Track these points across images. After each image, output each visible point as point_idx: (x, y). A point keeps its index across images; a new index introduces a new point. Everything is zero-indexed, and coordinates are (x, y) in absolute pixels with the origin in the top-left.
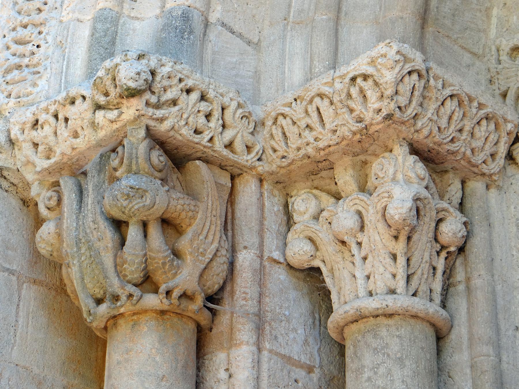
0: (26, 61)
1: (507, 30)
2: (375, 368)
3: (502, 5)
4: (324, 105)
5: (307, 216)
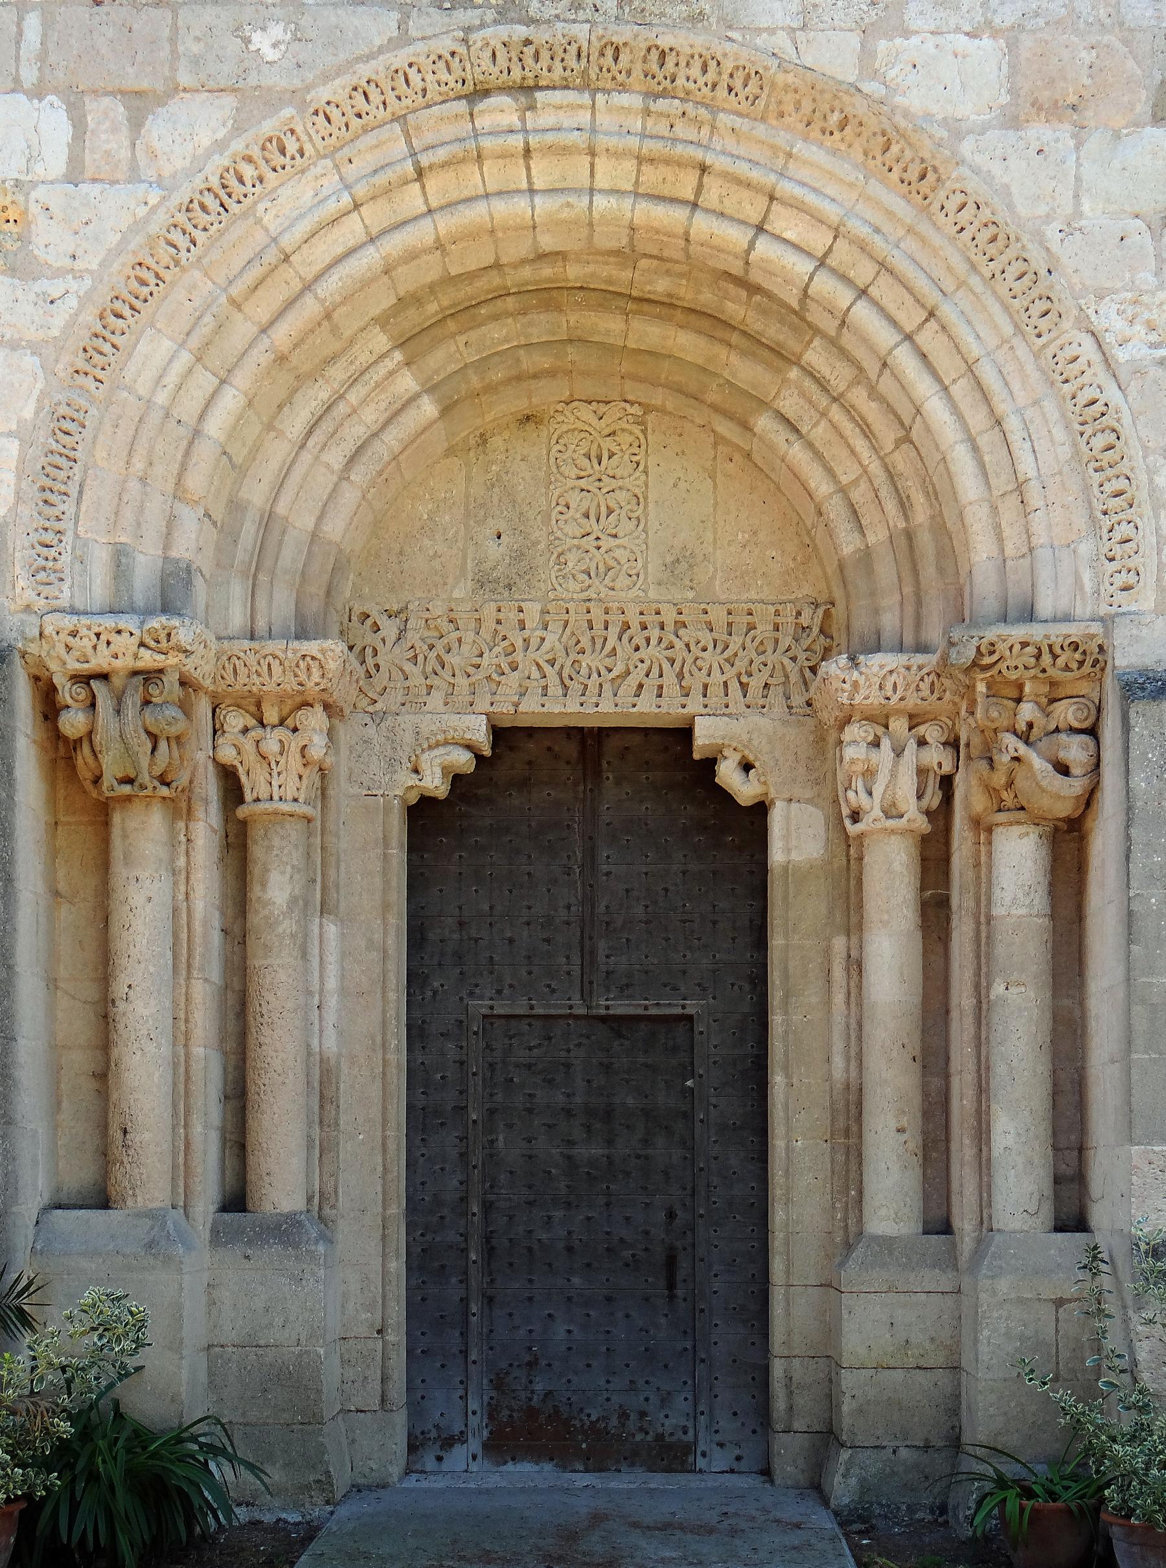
0: (50, 564)
2: (282, 849)
4: (275, 665)
5: (236, 730)
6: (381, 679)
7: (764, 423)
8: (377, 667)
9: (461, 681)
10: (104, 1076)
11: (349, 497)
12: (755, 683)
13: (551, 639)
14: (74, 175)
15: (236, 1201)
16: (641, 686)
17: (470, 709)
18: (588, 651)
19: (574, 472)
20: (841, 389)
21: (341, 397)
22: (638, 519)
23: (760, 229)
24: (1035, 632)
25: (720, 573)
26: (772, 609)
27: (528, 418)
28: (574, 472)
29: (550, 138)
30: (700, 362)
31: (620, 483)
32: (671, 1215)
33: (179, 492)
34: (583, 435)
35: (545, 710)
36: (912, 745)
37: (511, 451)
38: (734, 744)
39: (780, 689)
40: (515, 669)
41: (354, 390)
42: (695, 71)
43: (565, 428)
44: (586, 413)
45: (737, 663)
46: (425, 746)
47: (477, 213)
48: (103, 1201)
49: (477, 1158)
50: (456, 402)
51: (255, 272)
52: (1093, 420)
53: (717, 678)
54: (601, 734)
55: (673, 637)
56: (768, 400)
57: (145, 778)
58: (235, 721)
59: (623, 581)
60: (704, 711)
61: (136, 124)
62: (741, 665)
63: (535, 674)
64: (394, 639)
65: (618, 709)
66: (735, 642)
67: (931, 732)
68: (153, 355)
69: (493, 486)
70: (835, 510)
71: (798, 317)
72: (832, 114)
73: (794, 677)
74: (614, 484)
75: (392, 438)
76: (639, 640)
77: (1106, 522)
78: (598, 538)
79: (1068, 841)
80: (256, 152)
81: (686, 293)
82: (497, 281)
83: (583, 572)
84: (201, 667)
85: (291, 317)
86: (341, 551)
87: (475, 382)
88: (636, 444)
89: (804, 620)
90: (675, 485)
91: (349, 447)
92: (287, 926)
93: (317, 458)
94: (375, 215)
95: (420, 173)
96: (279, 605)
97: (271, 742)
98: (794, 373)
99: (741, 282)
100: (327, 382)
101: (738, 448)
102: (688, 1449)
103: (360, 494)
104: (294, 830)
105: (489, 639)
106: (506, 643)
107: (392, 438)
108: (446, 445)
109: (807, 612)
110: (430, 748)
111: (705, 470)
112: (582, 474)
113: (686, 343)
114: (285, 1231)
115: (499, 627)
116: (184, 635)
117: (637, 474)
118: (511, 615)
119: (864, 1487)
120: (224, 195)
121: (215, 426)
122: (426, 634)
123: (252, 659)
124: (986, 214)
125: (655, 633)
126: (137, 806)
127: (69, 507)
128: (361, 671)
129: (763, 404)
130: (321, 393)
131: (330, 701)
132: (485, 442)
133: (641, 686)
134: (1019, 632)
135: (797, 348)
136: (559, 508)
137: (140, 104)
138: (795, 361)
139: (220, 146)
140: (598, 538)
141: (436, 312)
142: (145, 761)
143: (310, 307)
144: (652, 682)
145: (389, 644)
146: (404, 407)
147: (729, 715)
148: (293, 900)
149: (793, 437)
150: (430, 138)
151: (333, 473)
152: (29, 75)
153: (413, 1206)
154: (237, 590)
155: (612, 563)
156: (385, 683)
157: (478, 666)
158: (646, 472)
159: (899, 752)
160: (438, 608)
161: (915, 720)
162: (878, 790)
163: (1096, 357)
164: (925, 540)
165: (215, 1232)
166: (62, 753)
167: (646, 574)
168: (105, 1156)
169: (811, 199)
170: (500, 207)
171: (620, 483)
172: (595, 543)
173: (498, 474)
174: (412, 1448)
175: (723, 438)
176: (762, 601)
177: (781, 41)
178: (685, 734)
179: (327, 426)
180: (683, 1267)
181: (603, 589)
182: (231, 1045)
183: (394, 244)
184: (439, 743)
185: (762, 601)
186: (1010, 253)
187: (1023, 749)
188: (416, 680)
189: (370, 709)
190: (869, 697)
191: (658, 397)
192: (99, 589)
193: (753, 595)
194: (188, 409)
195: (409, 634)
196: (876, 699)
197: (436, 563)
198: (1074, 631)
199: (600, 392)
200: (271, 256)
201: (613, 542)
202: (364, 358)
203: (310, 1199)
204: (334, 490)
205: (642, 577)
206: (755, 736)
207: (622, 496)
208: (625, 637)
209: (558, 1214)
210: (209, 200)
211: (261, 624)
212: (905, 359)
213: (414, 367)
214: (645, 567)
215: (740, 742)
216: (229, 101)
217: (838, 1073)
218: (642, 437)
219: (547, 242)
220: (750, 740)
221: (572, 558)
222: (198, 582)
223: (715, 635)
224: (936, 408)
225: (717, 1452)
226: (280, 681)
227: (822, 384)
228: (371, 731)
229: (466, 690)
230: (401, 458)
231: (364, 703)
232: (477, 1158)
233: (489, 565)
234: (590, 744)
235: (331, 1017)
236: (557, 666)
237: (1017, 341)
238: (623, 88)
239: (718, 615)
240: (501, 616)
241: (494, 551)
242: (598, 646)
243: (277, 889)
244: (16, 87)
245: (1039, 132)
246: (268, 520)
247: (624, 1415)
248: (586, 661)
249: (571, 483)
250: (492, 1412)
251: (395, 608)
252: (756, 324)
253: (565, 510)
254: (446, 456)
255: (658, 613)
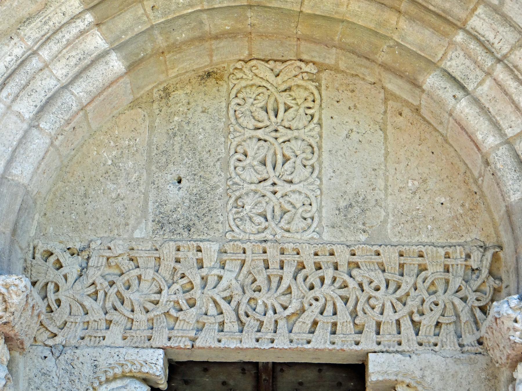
1: (44, 235)
3: (42, 214)
6: (61, 315)
7: (432, 81)
8: (59, 302)
9: (140, 316)
11: (38, 143)
12: (427, 322)
13: (228, 277)
16: (315, 323)
17: (147, 344)
18: (264, 289)
19: (252, 123)
20: (505, 51)
21: (35, 53)
22: (313, 167)
25: (391, 218)
26: (442, 252)
27: (209, 74)
28: (252, 123)
30: (372, 26)
31: (296, 133)
34: (261, 90)
35: (221, 345)
37: (193, 104)
38: (407, 381)
39: (452, 328)
40: (192, 306)
41: (47, 47)
43: (243, 83)
45: (409, 302)
46: (103, 379)
50: (142, 60)
53: (390, 316)
54: (276, 369)
55: (346, 277)
56: (436, 62)
59: (298, 224)
60: (378, 348)
62: (413, 304)
63: (212, 310)
64: (75, 276)
65: (294, 346)
66: (407, 282)
69: (175, 135)
73: (465, 317)
74: (290, 134)
75: (81, 90)
76: (314, 279)
78: (274, 184)
83: (260, 215)
86: (27, 193)
87: (161, 41)
88: (310, 99)
89: (474, 263)
90: (348, 136)
91: (40, 98)
93: (9, 107)
98: (460, 37)
100: (22, 39)
101: (407, 103)
103: (48, 141)
105: (168, 276)
106: (184, 281)
107: (81, 90)
108: (131, 98)
109: (476, 255)
110: (108, 381)
111: (376, 122)
112: (260, 125)
115: (178, 266)
117: (312, 126)
118: (190, 254)
122: (107, 271)
125: (329, 273)
128: (42, 306)
129: (431, 64)
131: (12, 334)
132: (168, 95)
133: (315, 323)
135: (463, 15)
136: (238, 156)
140: (274, 184)
144: (327, 318)
145: (71, 280)
146: (93, 62)
147: (401, 353)
149: (459, 94)
151: (23, 121)
155: (288, 207)
156: (65, 317)
157: (157, 303)
158: (320, 124)
160: (120, 247)
167: (320, 217)
171: (296, 133)
172: (272, 188)
173: (180, 124)
175: (393, 94)
176: (433, 245)
178: (357, 371)
179: (20, 79)
181: (278, 231)
185: (433, 245)
188: (96, 314)
189: (50, 342)
191: (331, 57)
193: (424, 239)
195: (91, 271)
197: (119, 206)
199: (278, 52)
201: (288, 188)
204: (24, 137)
205: (316, 220)
206: (427, 373)
207: (296, 145)
208: (300, 277)
213: (103, 27)
214: (319, 211)
215: (413, 378)
218: (316, 92)
220: (423, 377)
221: (249, 202)
223: (387, 275)
227: (487, 47)
228: (51, 363)
229: (144, 325)
230: (88, 108)
233: (170, 207)
236: (234, 304)
239: (389, 256)
240: (180, 255)
241: (174, 194)
242: (274, 285)
248: (261, 298)
249: (248, 133)
251: (78, 246)
253: (242, 157)
254: (131, 108)
255: (332, 254)
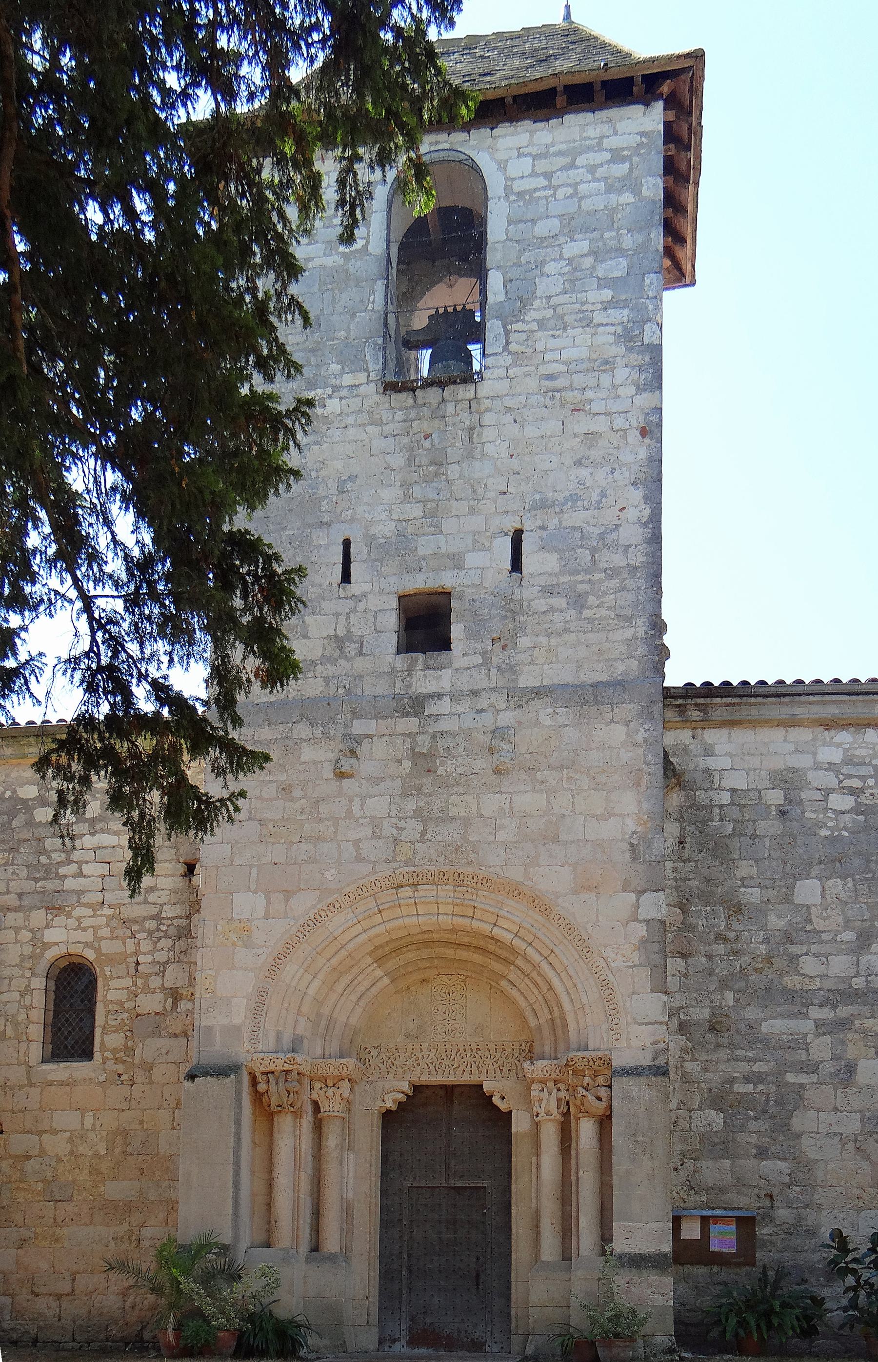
6: (371, 1070)
10: (269, 1205)
11: (359, 1010)
12: (505, 1069)
13: (432, 1055)
14: (266, 917)
15: (315, 1248)
23: (495, 925)
24: (587, 1054)
29: (423, 900)
32: (478, 1259)
33: (299, 1012)
36: (555, 1090)
42: (470, 878)
44: (444, 978)
47: (400, 922)
48: (268, 1245)
49: (406, 1238)
51: (325, 943)
52: (604, 985)
57: (285, 1105)
58: (318, 1085)
61: (287, 901)
66: (498, 1056)
67: (562, 1086)
68: (291, 970)
70: (528, 1012)
71: (512, 949)
72: (515, 891)
75: (373, 991)
77: (610, 1018)
79: (605, 1122)
80: (326, 908)
81: (475, 942)
82: (409, 939)
84: (306, 1068)
85: (337, 956)
87: (403, 971)
92: (335, 1154)
94: (366, 924)
95: (380, 912)
96: (334, 1046)
97: (330, 1093)
98: (512, 967)
99: (493, 938)
102: (484, 1344)
104: (338, 1122)
107: (373, 991)
113: (477, 958)
114: (331, 1258)
116: (299, 1059)
119: (537, 1348)
120: (315, 920)
121: (311, 992)
123: (323, 1065)
124: (567, 921)
125: (469, 1053)
126: (283, 1114)
127: (262, 1019)
130: (349, 977)
134: (581, 1054)
137: (288, 894)
138: (512, 963)
139: (314, 906)
141: (385, 952)
142: (285, 1100)
143: (344, 953)
144: (468, 1069)
148: (337, 1145)
150: (384, 901)
152: (253, 887)
153: (382, 1256)
154: (319, 1042)
159: (550, 1093)
160: (392, 1046)
161: (556, 1082)
162: (543, 1106)
163: (605, 966)
164: (558, 1021)
165: (307, 1259)
166: (258, 1098)
168: (269, 1231)
169: (510, 916)
170: (407, 921)
174: (380, 1343)
177: (498, 869)
180: (482, 1276)
182: (315, 1196)
183: (372, 933)
184: (392, 1092)
186: (576, 933)
187: (585, 1092)
190: (538, 1075)
191: (469, 974)
192: (271, 1044)
194: (303, 986)
196: (541, 1075)
198: (600, 1054)
200: (330, 939)
202: (363, 966)
203: (341, 1249)
207: (457, 1006)
209: (436, 1258)
210: (310, 923)
211: (327, 1054)
212: (544, 965)
216: (317, 893)
217: (533, 1205)
219: (425, 928)
222: (305, 1041)
224: (556, 982)
225: (494, 1346)
226: (332, 1072)
227: (522, 972)
231: (365, 1078)
232: (406, 1238)
234: (449, 1091)
235: (351, 1186)
237: (580, 960)
238: (447, 884)
239: (492, 1046)
241: (412, 1026)
243: (332, 1141)
244: (249, 890)
245: (585, 896)
246: (330, 1019)
247: (459, 1332)
248: (444, 1062)
250: (410, 1330)
252: (499, 951)
